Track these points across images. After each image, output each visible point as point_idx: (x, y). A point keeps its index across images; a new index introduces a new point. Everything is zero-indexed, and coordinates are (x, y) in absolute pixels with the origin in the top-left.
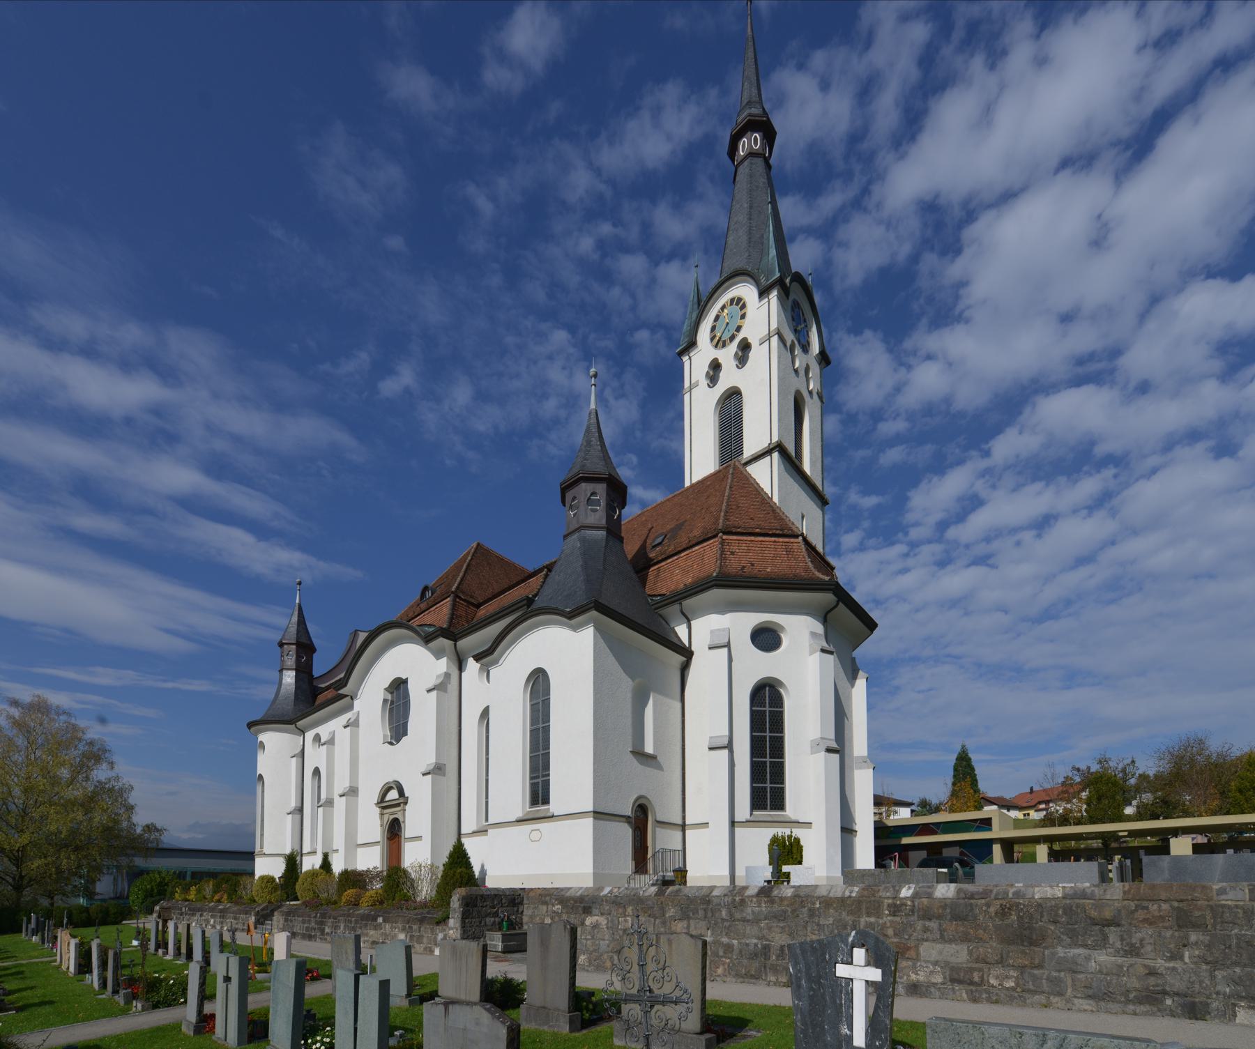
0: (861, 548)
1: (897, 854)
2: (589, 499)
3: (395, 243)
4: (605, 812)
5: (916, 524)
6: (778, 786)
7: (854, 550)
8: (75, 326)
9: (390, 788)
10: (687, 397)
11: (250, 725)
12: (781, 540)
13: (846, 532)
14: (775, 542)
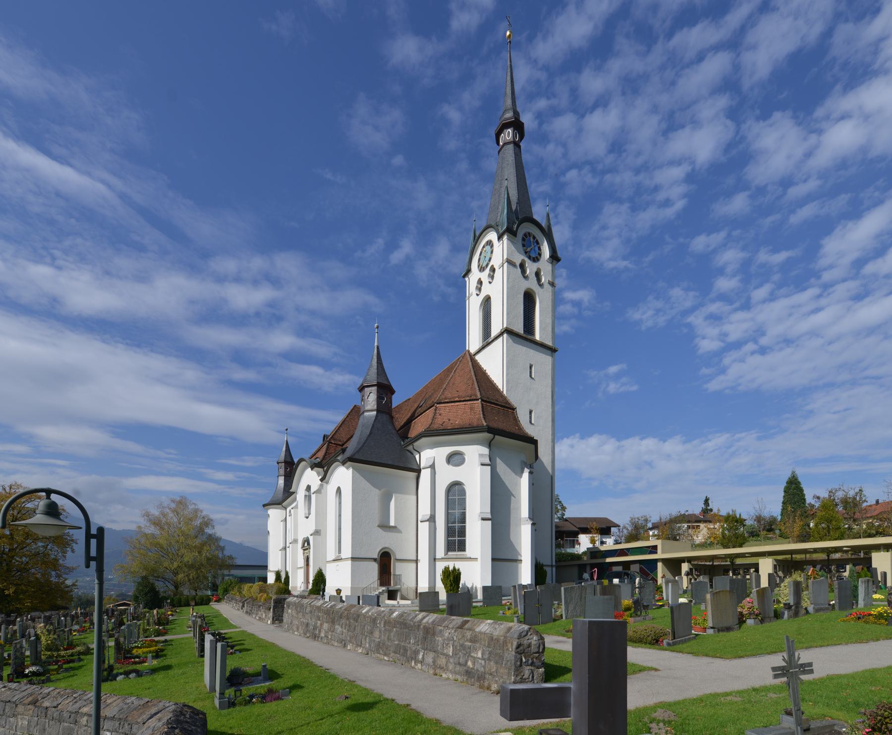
0: (772, 297)
1: (596, 569)
3: (398, 160)
4: (360, 557)
5: (831, 267)
6: (462, 538)
7: (764, 301)
8: (229, 265)
10: (467, 302)
11: (264, 506)
13: (756, 288)
14: (465, 404)
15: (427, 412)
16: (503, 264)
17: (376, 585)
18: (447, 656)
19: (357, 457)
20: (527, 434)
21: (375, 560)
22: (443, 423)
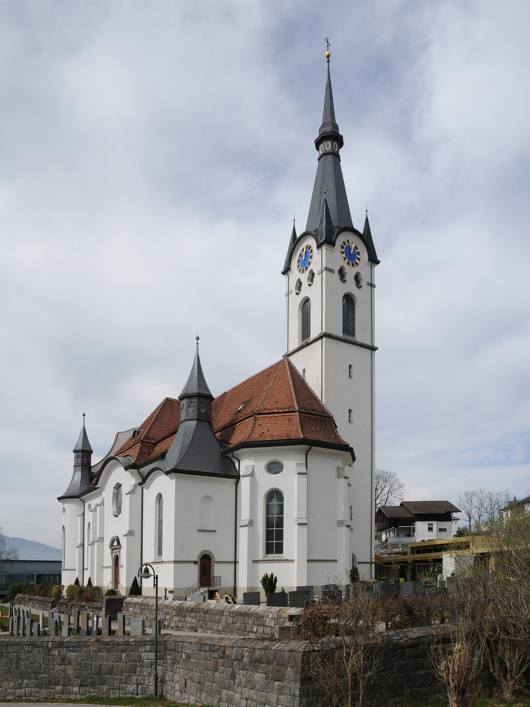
2: (189, 405)
9: (114, 540)
12: (287, 414)
14: (284, 416)
15: (247, 420)
16: (322, 272)
17: (196, 586)
18: (271, 627)
19: (180, 468)
20: (343, 441)
21: (195, 562)
22: (262, 434)
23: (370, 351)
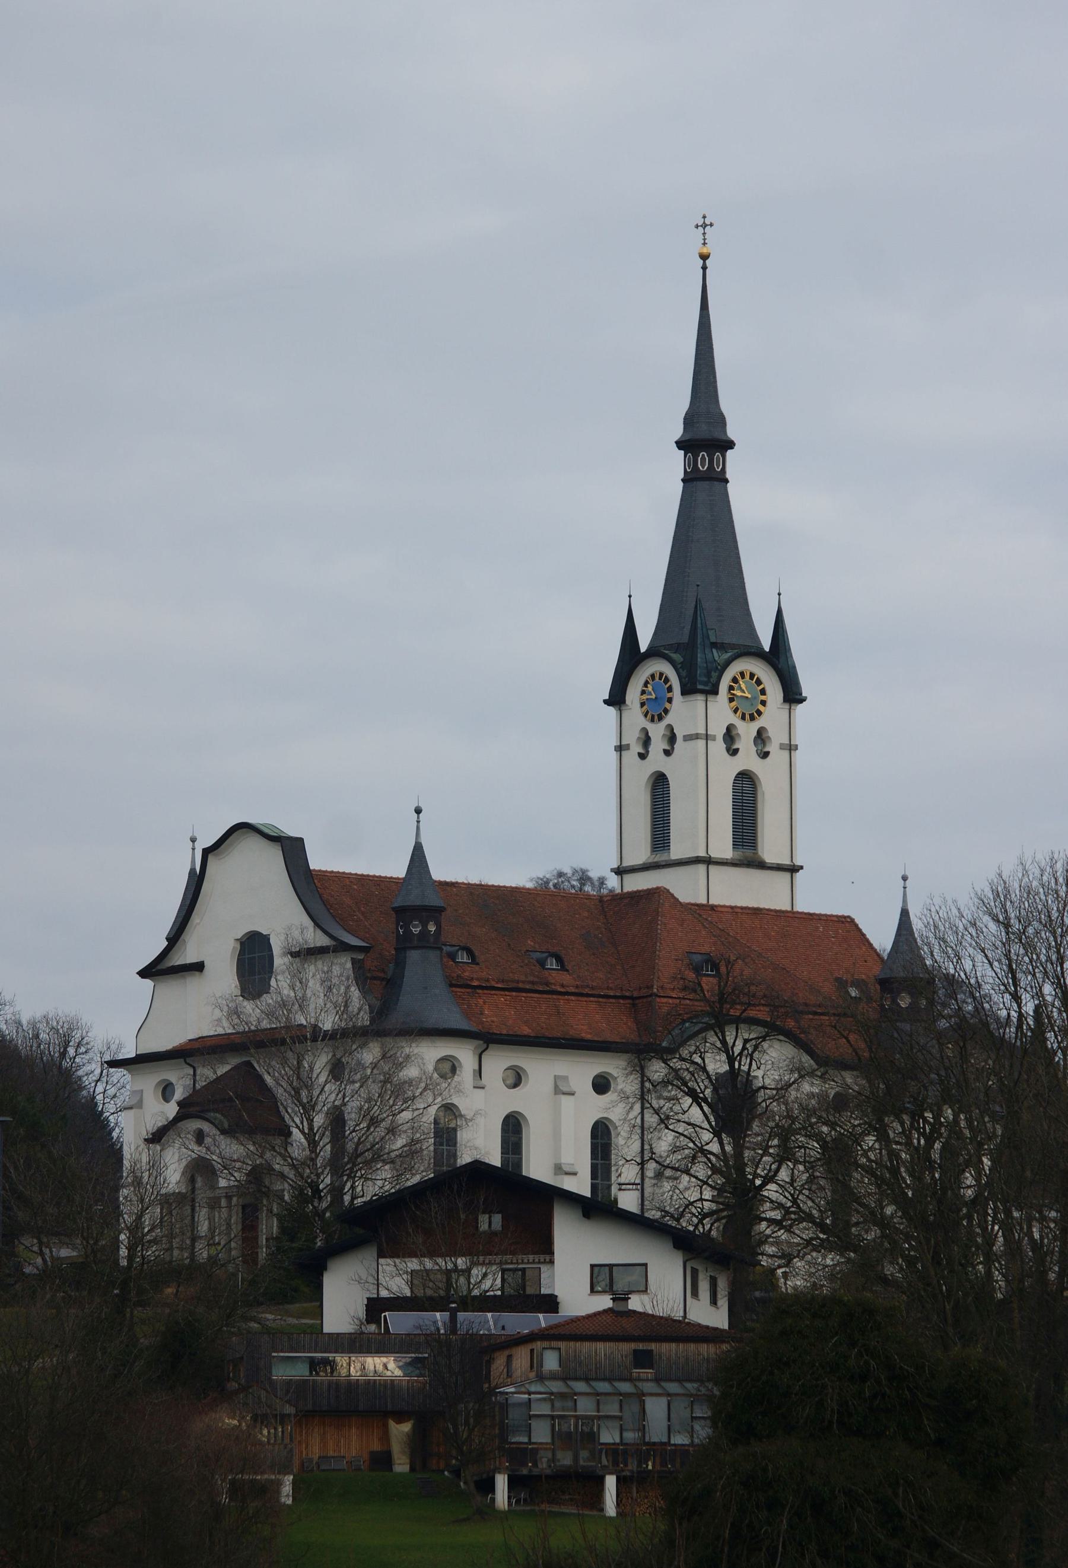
21: (685, 1317)
23: (788, 875)
